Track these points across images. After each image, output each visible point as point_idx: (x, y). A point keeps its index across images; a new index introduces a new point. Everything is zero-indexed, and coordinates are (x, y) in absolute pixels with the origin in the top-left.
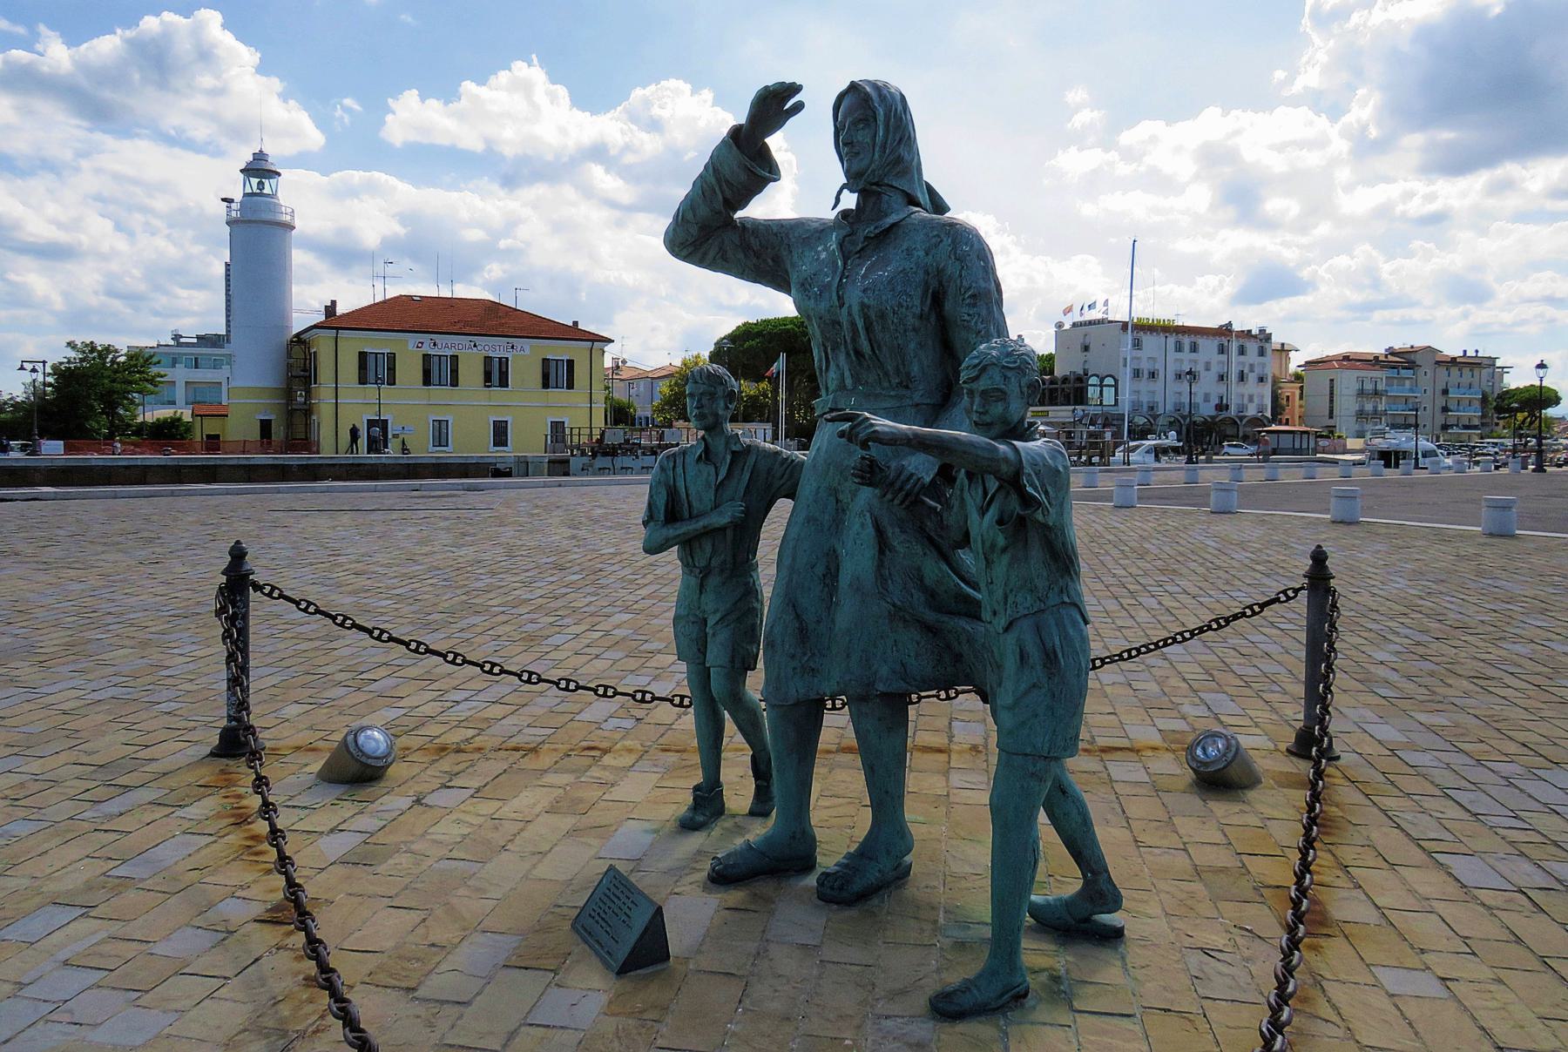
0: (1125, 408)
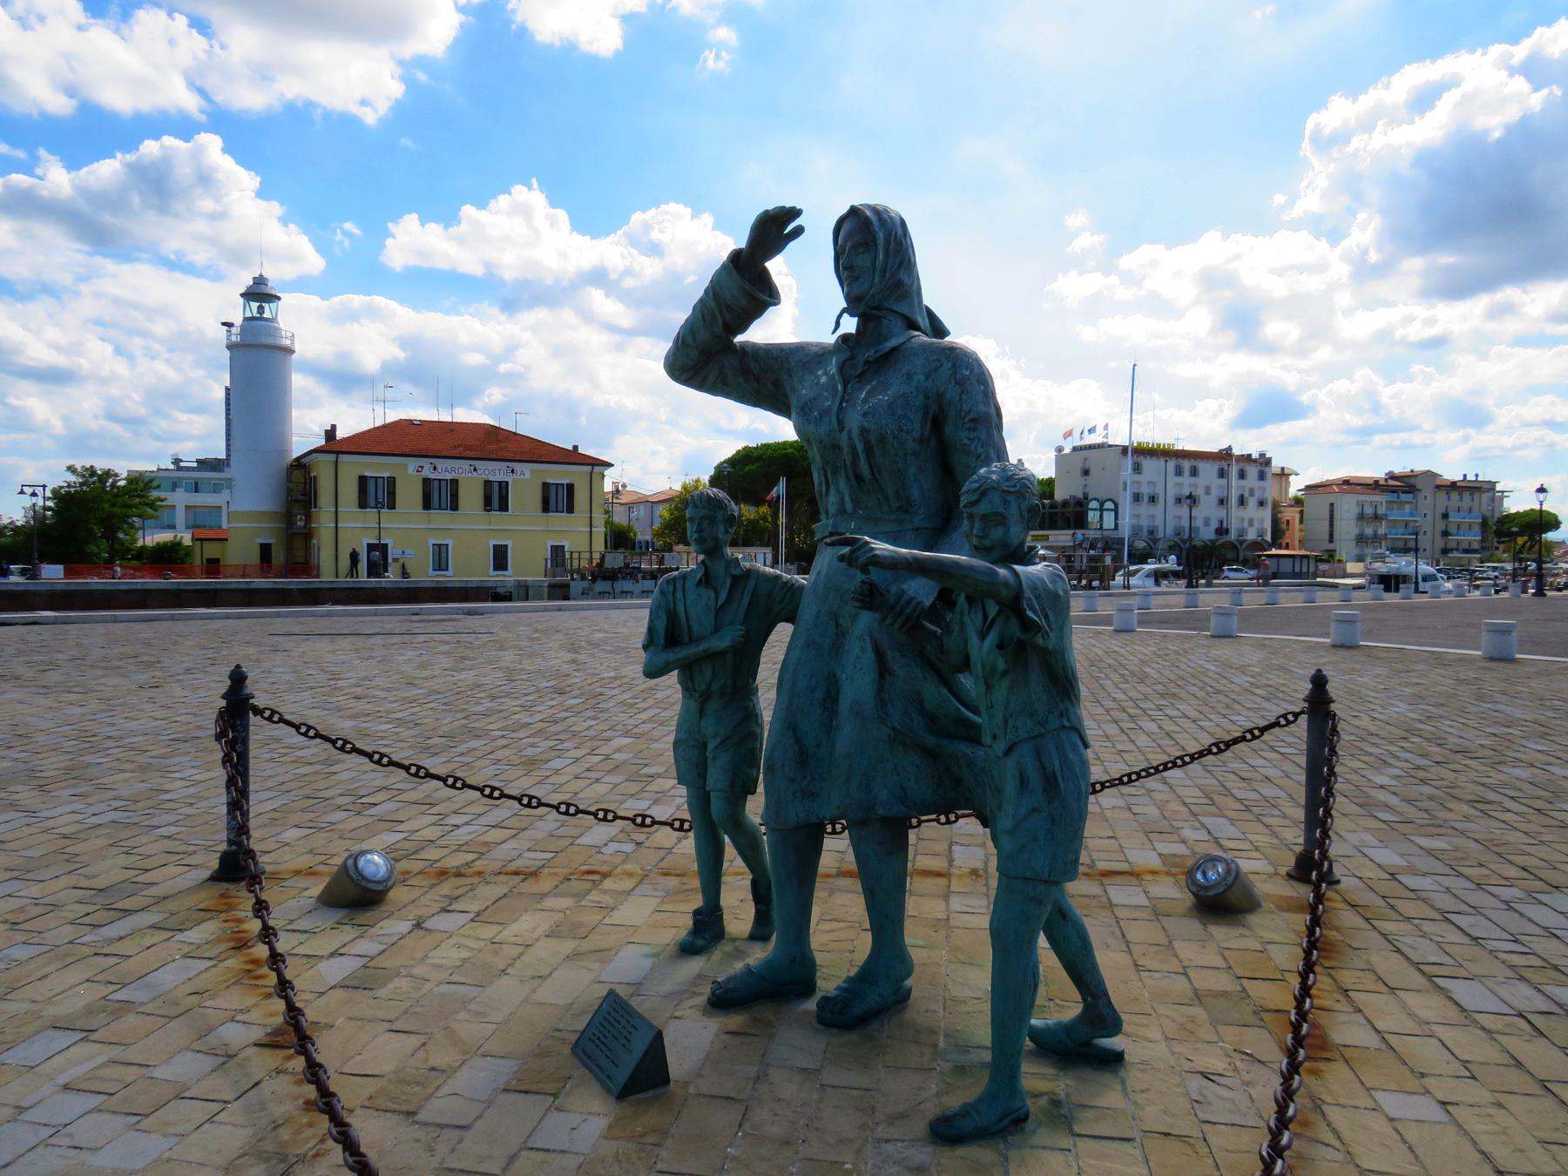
0: (1125, 532)
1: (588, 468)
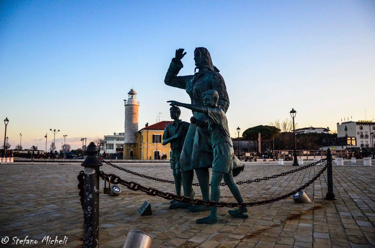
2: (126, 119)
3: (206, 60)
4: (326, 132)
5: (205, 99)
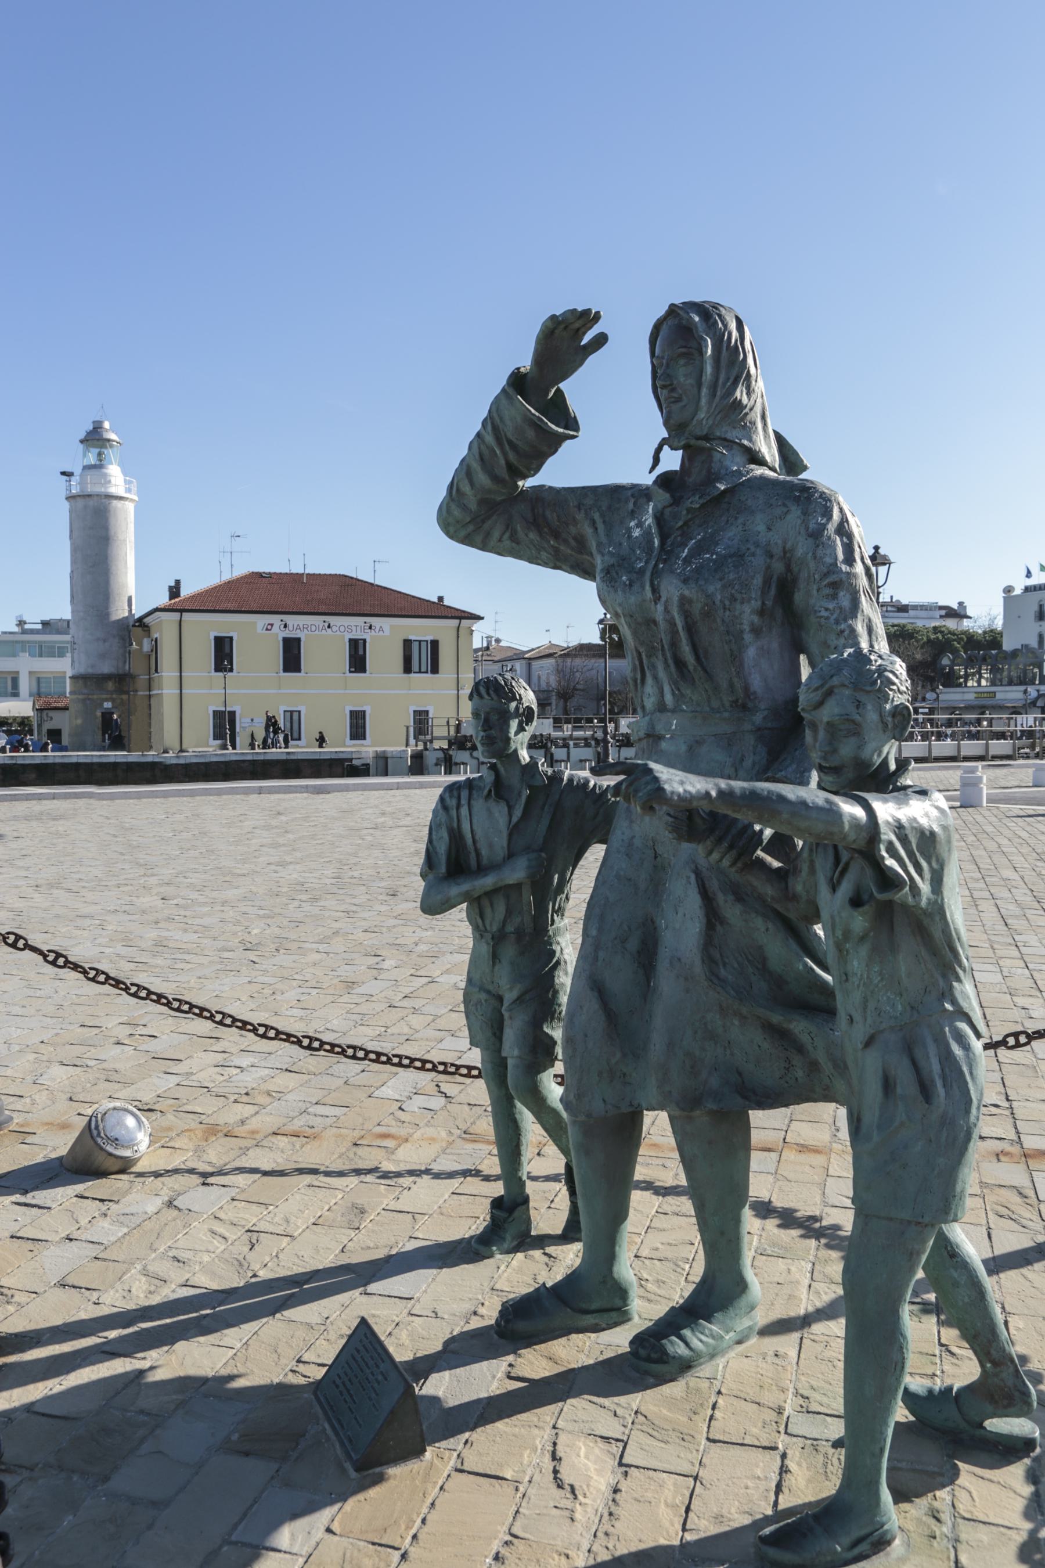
1: (456, 622)
2: (74, 562)
3: (738, 394)
4: (951, 624)
5: (831, 727)
